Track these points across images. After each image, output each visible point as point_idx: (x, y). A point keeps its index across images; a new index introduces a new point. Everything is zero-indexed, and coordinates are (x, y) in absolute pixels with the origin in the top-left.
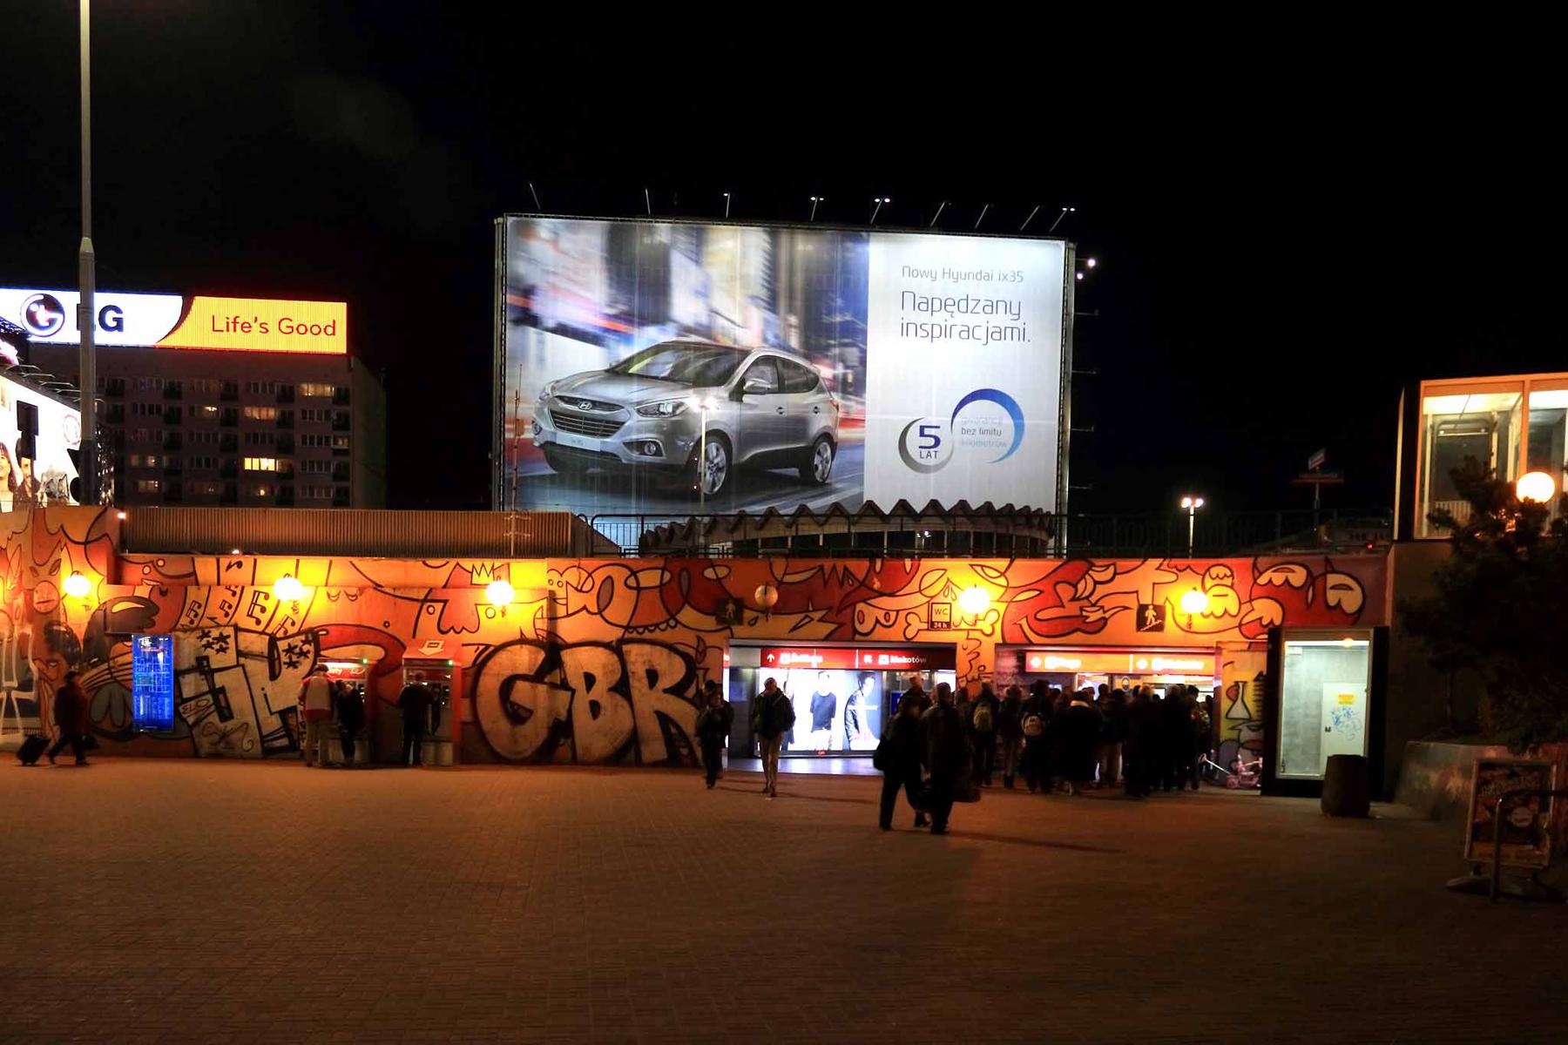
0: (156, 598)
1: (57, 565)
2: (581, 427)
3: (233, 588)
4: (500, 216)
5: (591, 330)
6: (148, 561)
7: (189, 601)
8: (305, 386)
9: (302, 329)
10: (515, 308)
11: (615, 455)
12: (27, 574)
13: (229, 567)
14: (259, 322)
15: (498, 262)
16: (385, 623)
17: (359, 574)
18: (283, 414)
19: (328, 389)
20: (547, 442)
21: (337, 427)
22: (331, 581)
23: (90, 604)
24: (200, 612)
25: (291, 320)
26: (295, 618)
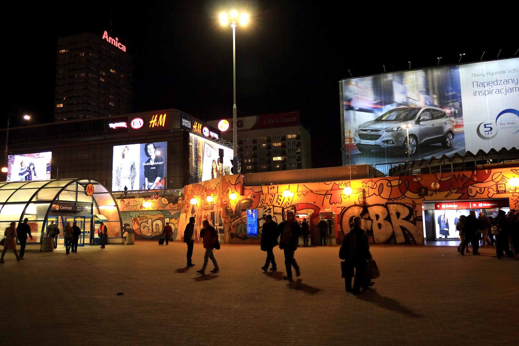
2: (368, 138)
5: (369, 109)
8: (288, 135)
10: (346, 105)
11: (379, 145)
12: (221, 194)
13: (271, 189)
15: (340, 93)
18: (283, 144)
20: (358, 144)
22: (299, 190)
24: (264, 202)
26: (289, 202)
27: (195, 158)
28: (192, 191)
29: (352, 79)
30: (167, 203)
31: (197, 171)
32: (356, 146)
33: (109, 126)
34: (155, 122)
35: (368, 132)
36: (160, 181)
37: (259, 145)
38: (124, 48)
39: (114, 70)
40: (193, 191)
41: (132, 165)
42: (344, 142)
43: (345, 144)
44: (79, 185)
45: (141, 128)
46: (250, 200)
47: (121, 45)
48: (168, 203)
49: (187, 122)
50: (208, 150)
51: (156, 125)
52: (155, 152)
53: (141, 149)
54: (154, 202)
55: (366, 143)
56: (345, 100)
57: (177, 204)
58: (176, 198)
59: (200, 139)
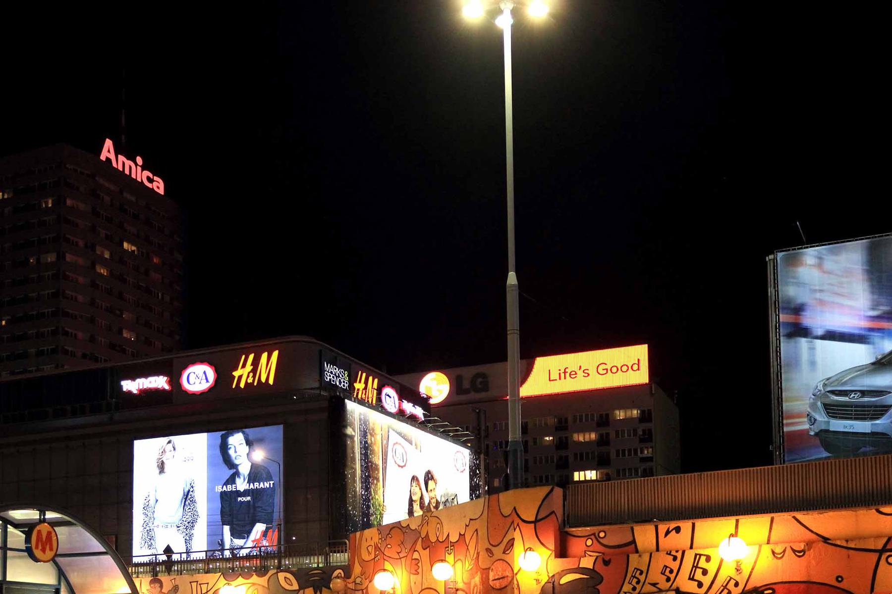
0: (601, 569)
1: (511, 544)
2: (851, 414)
3: (673, 553)
4: (771, 254)
5: (856, 332)
6: (590, 533)
7: (631, 569)
8: (617, 412)
9: (614, 370)
10: (787, 324)
11: (886, 434)
12: (483, 554)
13: (668, 533)
14: (583, 369)
15: (771, 290)
16: (838, 577)
17: (803, 528)
18: (601, 436)
19: (635, 412)
20: (821, 431)
21: (642, 441)
22: (772, 539)
23: (540, 578)
24: (642, 578)
25: (606, 364)
26: (738, 578)
27: (362, 471)
28: (377, 548)
29: (805, 248)
30: (296, 586)
31: (368, 507)
32: (818, 438)
33: (121, 387)
34: (249, 373)
35: (854, 398)
36: (265, 534)
37: (535, 443)
38: (159, 186)
39: (133, 244)
40: (382, 549)
41: (186, 490)
42: (781, 425)
43: (783, 432)
44: (10, 529)
45: (211, 389)
46: (590, 572)
47: (151, 175)
48: (298, 588)
49: (337, 371)
50: (397, 446)
51: (250, 380)
52: (248, 454)
53: (210, 447)
54: (254, 584)
55: (845, 427)
56: (784, 308)
57: (327, 590)
58: (324, 572)
59: (375, 418)
